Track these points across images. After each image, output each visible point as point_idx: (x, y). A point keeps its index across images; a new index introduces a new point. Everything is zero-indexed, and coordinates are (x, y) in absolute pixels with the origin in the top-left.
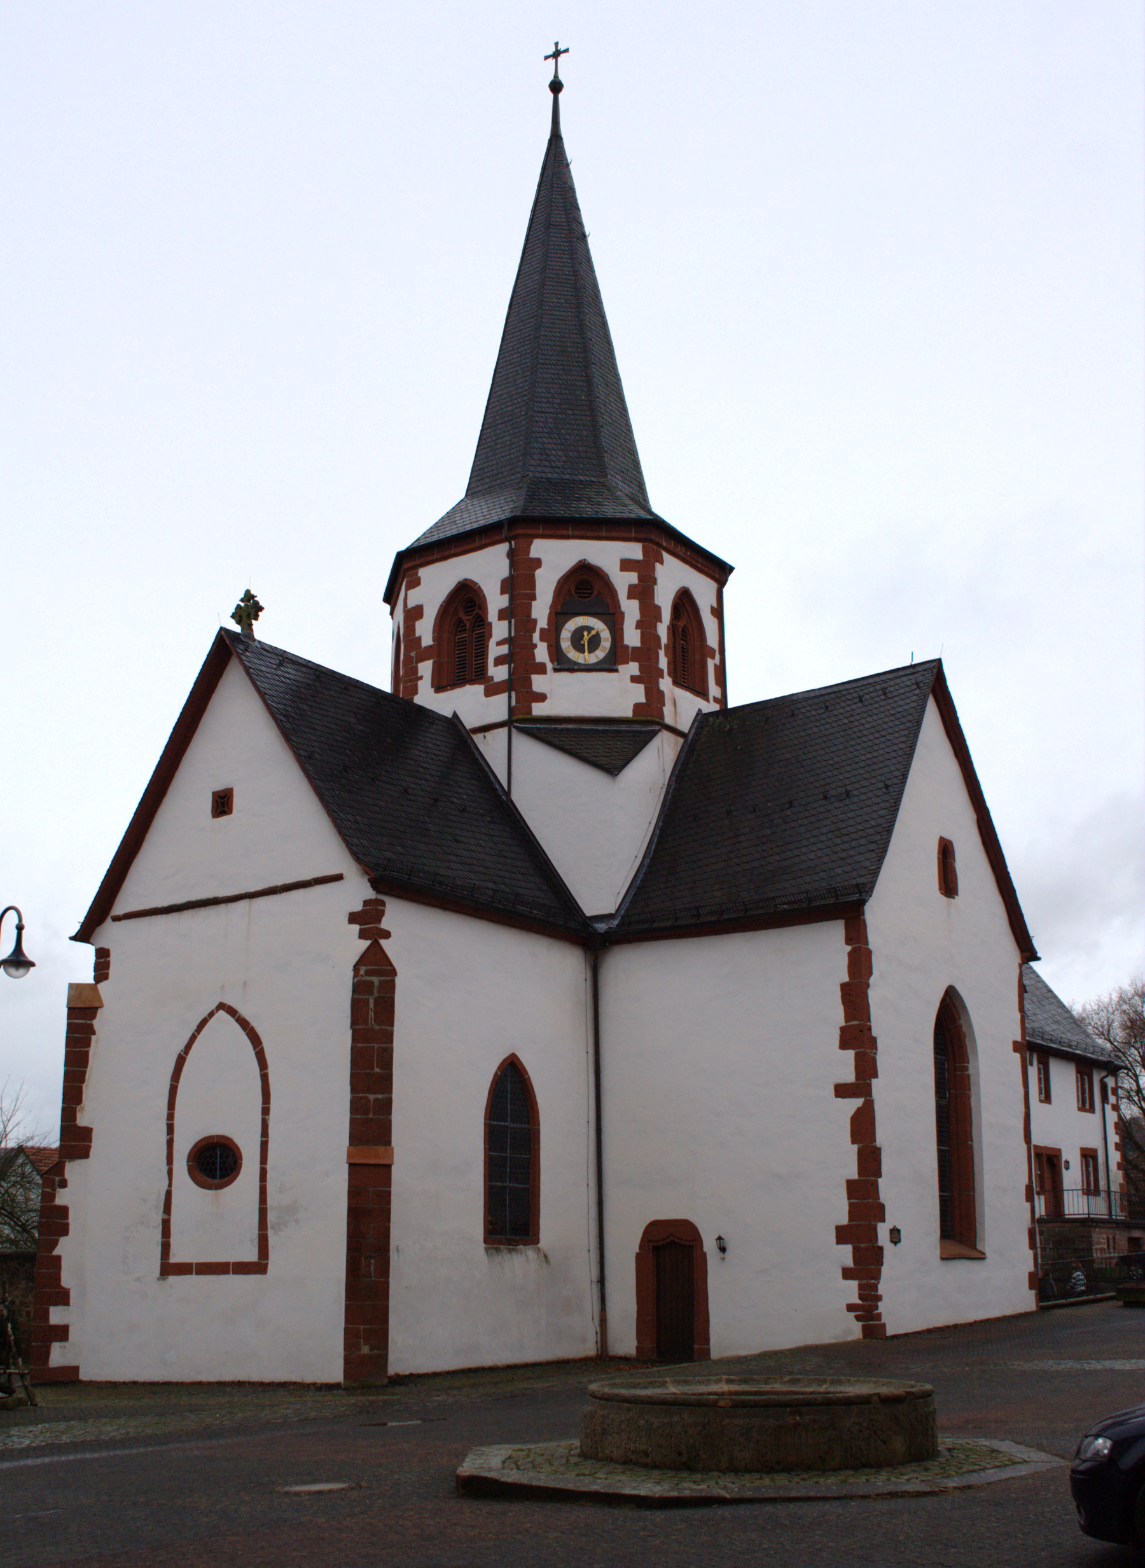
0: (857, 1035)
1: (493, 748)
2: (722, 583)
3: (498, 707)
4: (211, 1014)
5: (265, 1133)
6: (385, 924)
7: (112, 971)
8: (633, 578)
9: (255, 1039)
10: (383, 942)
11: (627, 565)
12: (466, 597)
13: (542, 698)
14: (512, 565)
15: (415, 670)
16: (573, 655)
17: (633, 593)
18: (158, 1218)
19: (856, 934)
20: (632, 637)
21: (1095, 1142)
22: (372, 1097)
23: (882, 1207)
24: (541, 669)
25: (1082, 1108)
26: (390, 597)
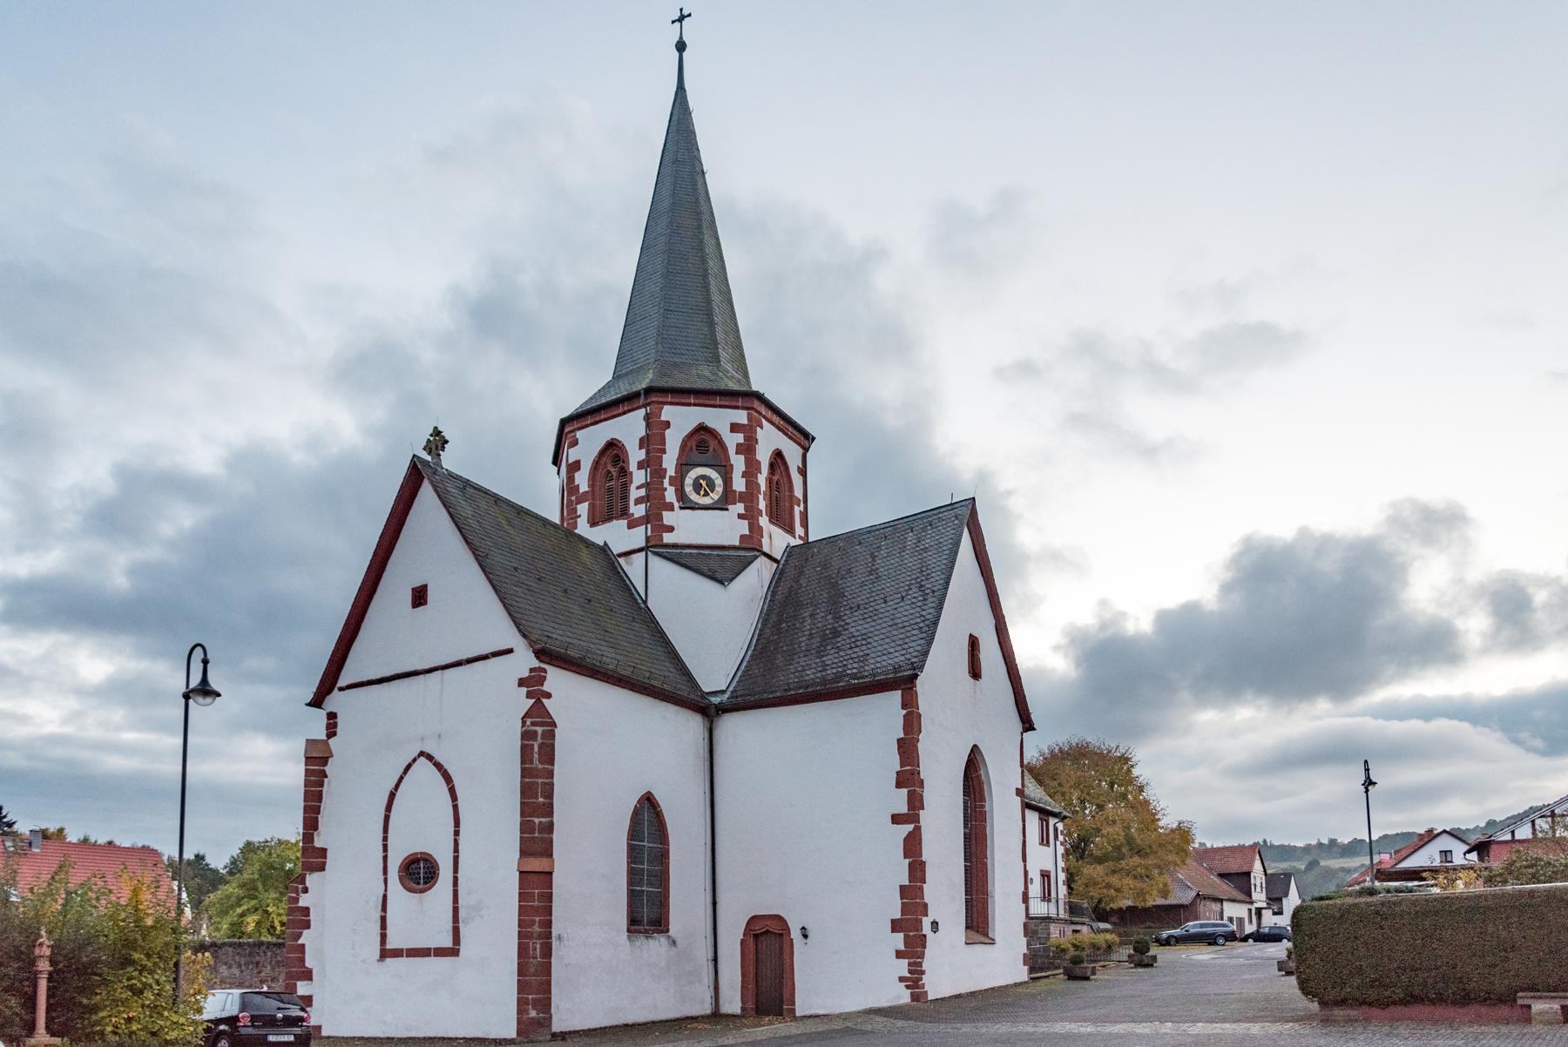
0: (909, 778)
1: (634, 569)
2: (806, 450)
3: (638, 537)
4: (414, 760)
5: (456, 850)
6: (546, 687)
7: (339, 730)
8: (740, 438)
9: (448, 778)
10: (545, 701)
11: (735, 428)
12: (613, 450)
13: (671, 529)
14: (648, 426)
15: (575, 510)
16: (694, 497)
17: (740, 449)
18: (379, 914)
19: (909, 702)
20: (739, 485)
21: (1050, 867)
22: (537, 820)
23: (926, 905)
24: (670, 507)
25: (1042, 843)
26: (556, 461)
